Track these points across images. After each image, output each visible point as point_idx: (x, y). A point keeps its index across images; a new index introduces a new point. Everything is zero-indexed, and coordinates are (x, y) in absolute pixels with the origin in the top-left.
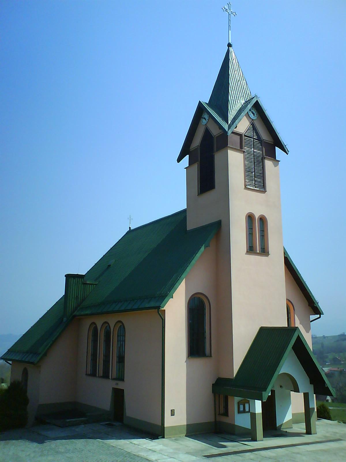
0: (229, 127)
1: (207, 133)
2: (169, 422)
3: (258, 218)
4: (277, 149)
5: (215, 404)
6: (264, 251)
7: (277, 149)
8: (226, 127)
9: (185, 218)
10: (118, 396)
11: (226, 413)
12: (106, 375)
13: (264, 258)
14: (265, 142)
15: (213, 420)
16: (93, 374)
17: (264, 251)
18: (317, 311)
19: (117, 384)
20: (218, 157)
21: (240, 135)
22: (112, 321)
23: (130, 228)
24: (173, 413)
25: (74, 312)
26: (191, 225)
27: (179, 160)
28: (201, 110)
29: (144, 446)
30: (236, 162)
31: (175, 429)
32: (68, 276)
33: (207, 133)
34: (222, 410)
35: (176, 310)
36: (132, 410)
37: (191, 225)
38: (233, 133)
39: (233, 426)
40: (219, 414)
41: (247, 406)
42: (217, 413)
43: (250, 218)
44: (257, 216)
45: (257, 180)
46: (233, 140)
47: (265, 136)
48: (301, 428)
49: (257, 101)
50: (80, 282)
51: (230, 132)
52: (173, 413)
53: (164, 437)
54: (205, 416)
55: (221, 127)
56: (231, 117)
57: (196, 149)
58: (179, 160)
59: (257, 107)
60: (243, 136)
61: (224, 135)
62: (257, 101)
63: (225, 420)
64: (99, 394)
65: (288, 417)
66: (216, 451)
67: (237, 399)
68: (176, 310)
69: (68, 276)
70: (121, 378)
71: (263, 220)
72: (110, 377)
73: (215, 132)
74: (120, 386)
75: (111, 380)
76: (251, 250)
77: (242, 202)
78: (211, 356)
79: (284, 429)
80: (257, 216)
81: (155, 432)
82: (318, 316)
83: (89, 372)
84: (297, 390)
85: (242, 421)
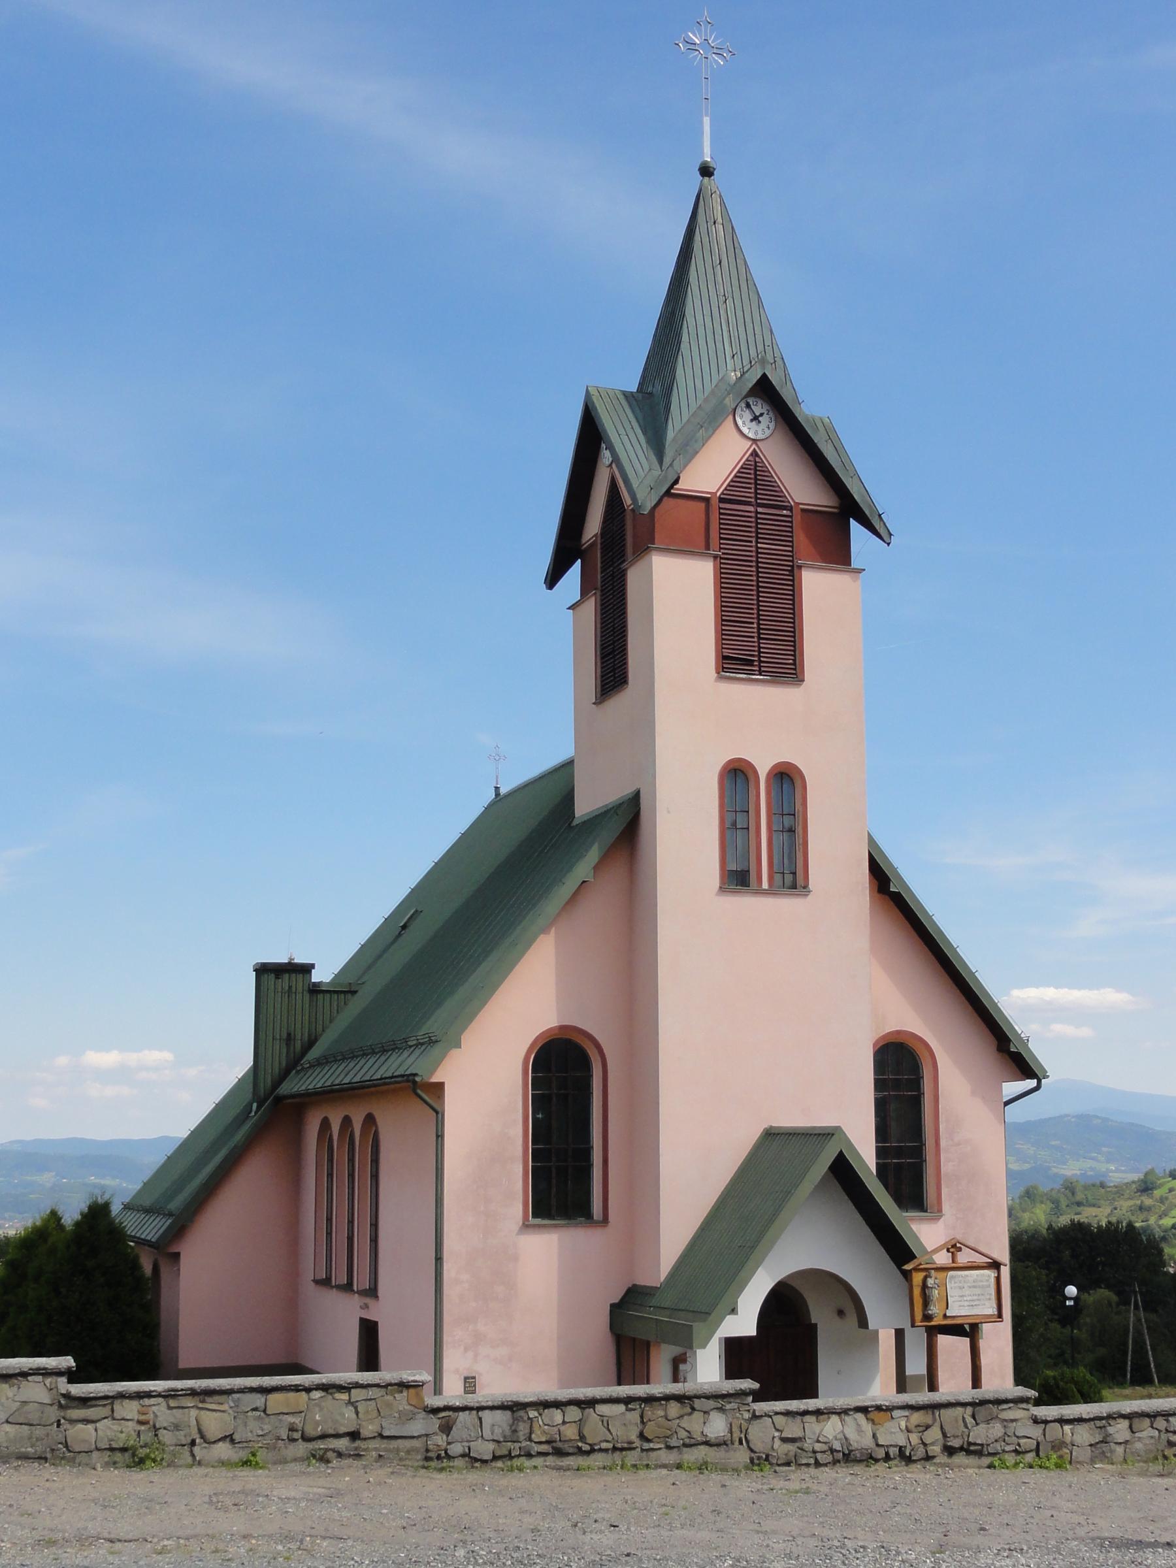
3: (768, 774)
4: (854, 524)
6: (792, 878)
9: (571, 777)
13: (786, 905)
14: (803, 510)
18: (1022, 1066)
19: (366, 1306)
20: (633, 576)
21: (707, 500)
23: (497, 788)
27: (552, 579)
32: (262, 970)
43: (737, 774)
47: (800, 488)
49: (764, 376)
50: (300, 989)
57: (592, 545)
58: (552, 579)
60: (715, 503)
62: (764, 376)
69: (262, 970)
70: (372, 1292)
71: (786, 777)
76: (738, 879)
78: (605, 1220)
82: (1032, 1083)
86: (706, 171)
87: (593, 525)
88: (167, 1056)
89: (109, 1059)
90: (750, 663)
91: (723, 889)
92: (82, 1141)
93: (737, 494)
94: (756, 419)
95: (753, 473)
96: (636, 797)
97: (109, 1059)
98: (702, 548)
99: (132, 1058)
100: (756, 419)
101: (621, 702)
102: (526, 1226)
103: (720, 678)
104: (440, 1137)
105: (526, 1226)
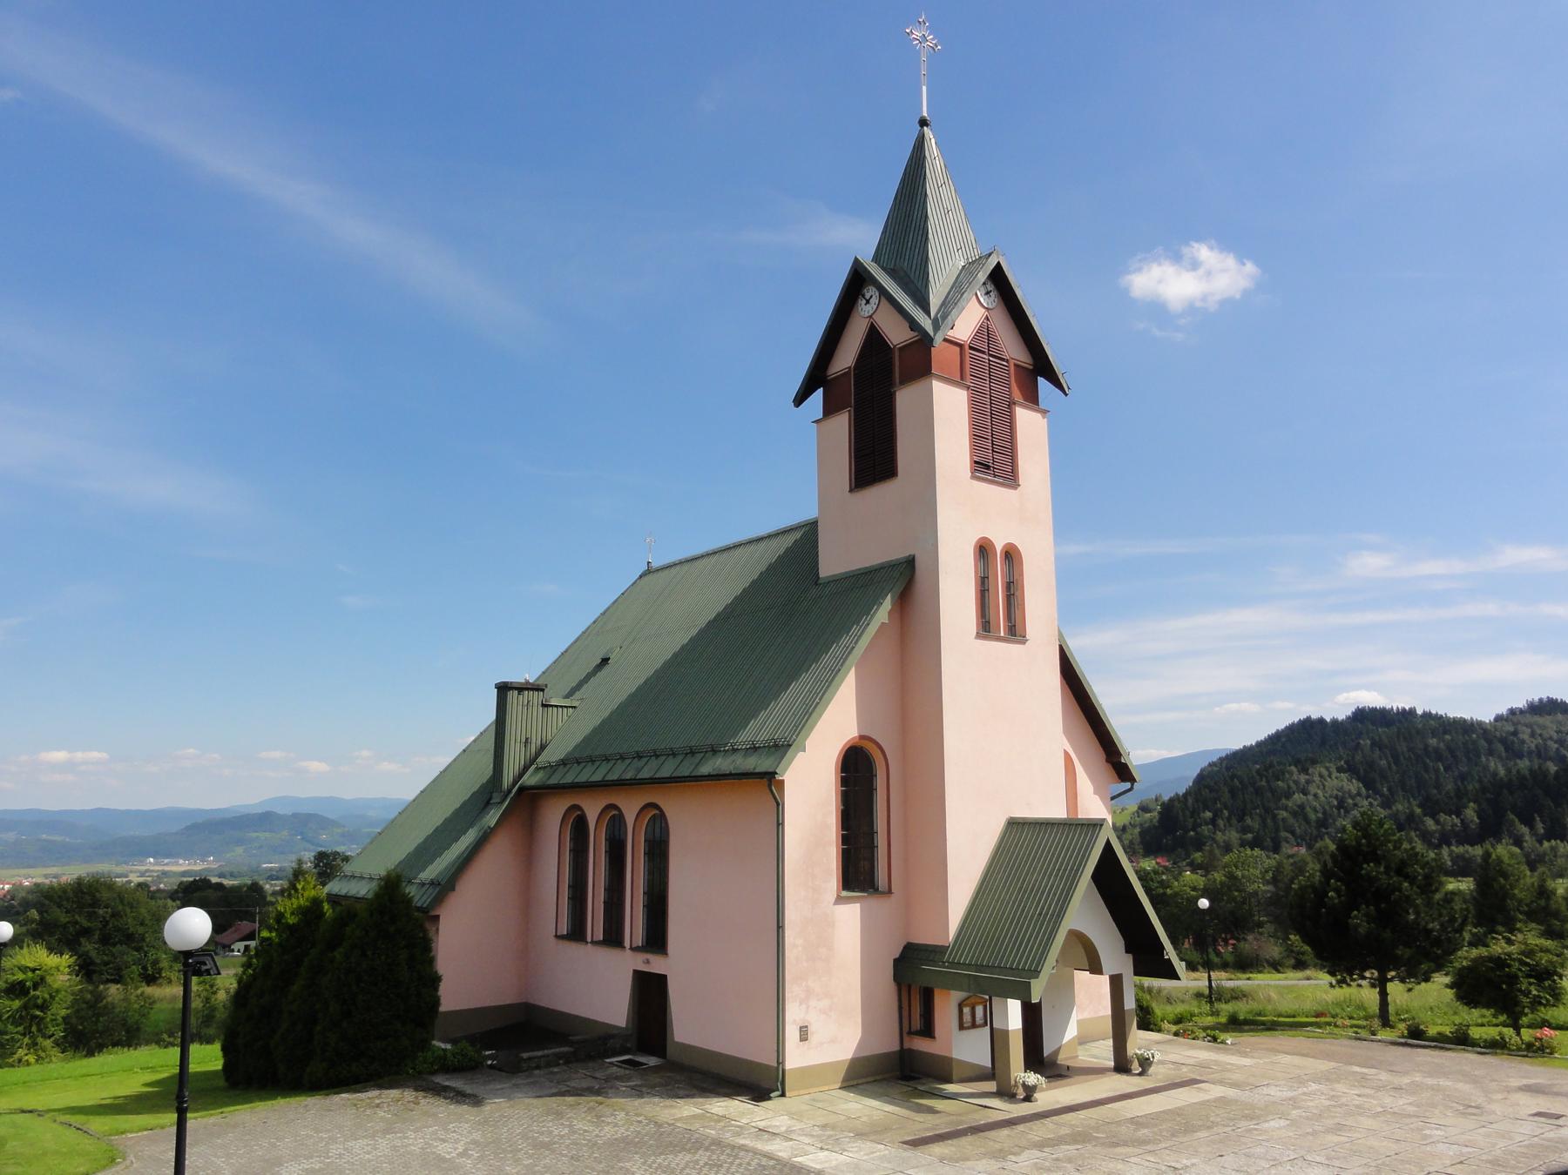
0: (937, 327)
1: (874, 338)
2: (796, 1057)
5: (900, 1008)
6: (1015, 632)
7: (1042, 382)
8: (927, 324)
10: (651, 994)
11: (928, 1031)
12: (613, 938)
15: (896, 1048)
16: (577, 933)
17: (1015, 632)
20: (904, 398)
21: (961, 346)
22: (630, 807)
24: (804, 1034)
25: (521, 775)
26: (831, 563)
27: (800, 399)
28: (858, 281)
29: (744, 1121)
30: (947, 412)
31: (812, 1074)
33: (874, 338)
34: (917, 1024)
35: (810, 787)
36: (690, 1025)
37: (831, 563)
38: (946, 340)
39: (948, 1061)
40: (910, 1033)
41: (979, 1010)
42: (906, 1029)
43: (983, 550)
44: (999, 548)
45: (995, 460)
46: (941, 354)
47: (1012, 348)
48: (1103, 1052)
51: (938, 340)
52: (804, 1034)
53: (783, 1095)
54: (888, 1043)
55: (914, 325)
56: (935, 302)
57: (846, 375)
58: (800, 399)
59: (998, 279)
61: (923, 343)
63: (921, 1045)
64: (598, 987)
65: (1071, 1032)
66: (923, 1124)
67: (956, 996)
68: (810, 787)
71: (1011, 555)
72: (627, 943)
73: (897, 334)
74: (656, 965)
75: (628, 952)
76: (986, 628)
77: (964, 514)
78: (890, 892)
79: (1062, 1059)
80: (999, 548)
81: (759, 1083)
82: (1128, 785)
83: (564, 931)
84: (1095, 968)
85: (971, 1048)
86: (923, 123)
87: (846, 357)
88: (105, 755)
89: (60, 756)
90: (988, 467)
91: (978, 636)
92: (39, 811)
93: (977, 345)
94: (988, 293)
95: (985, 332)
96: (910, 563)
97: (60, 756)
98: (960, 382)
99: (79, 755)
100: (988, 293)
101: (878, 494)
102: (839, 900)
103: (974, 477)
104: (780, 824)
105: (839, 900)
